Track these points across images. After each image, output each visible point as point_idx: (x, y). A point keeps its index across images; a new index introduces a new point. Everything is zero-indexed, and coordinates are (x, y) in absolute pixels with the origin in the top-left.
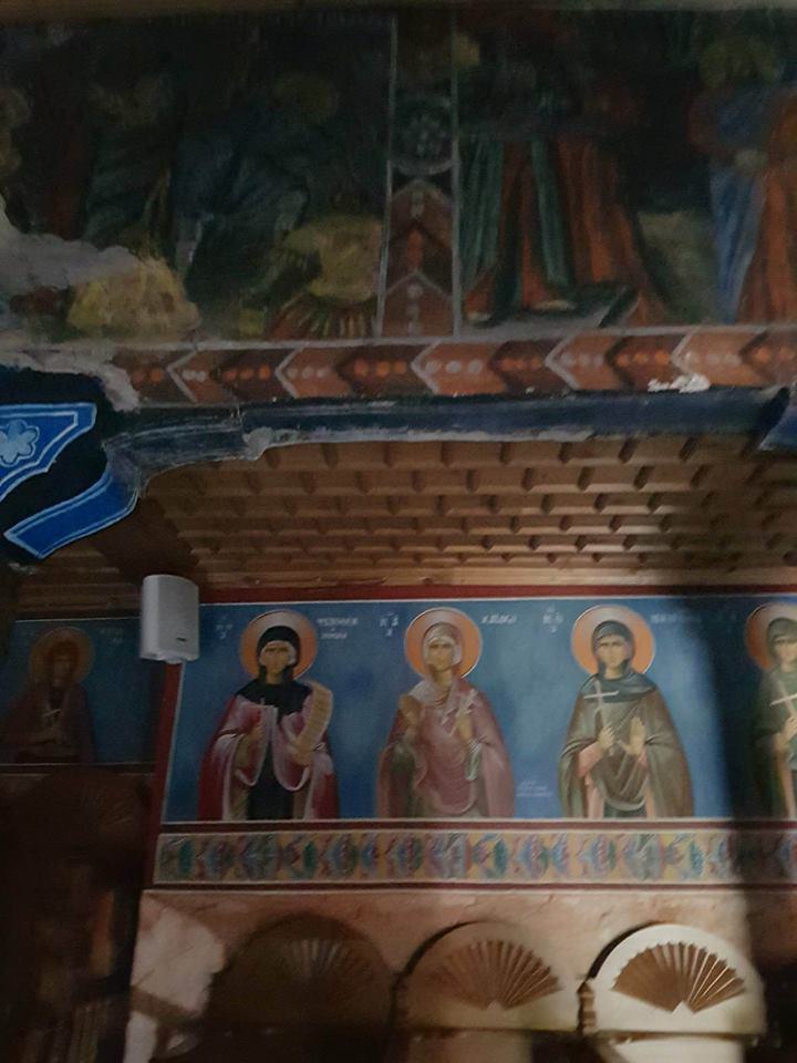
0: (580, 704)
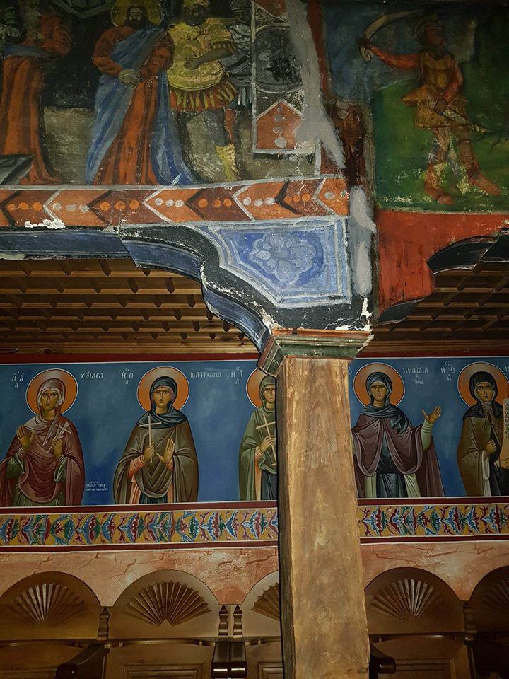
0: (137, 429)
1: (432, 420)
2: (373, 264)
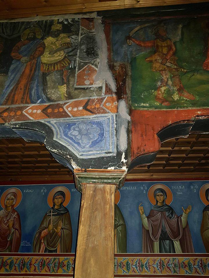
1: (187, 213)
2: (128, 135)
